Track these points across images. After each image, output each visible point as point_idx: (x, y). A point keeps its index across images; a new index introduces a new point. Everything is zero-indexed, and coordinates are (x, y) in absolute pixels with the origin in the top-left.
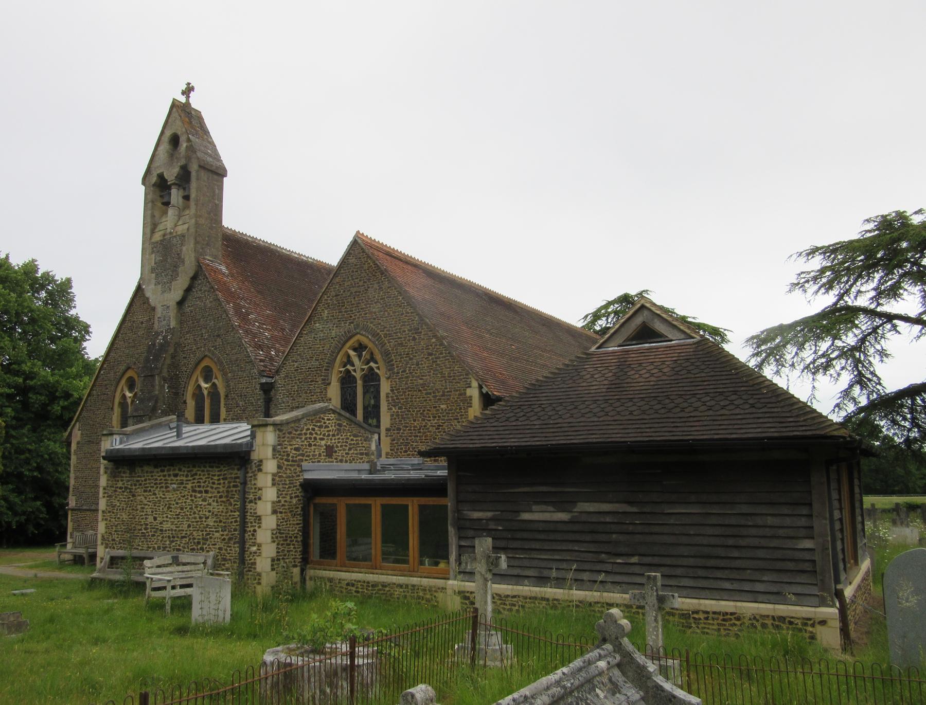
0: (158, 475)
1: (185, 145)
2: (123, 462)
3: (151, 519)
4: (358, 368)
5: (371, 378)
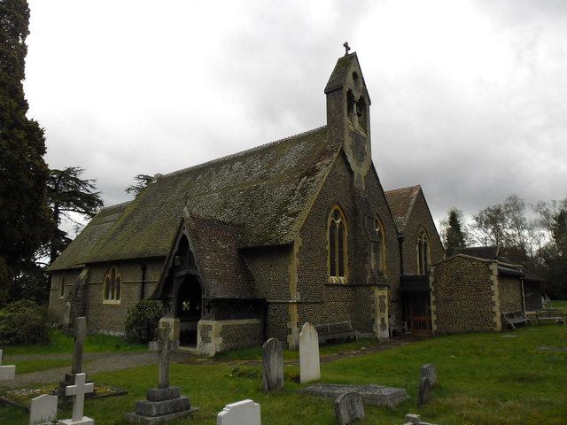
5: (425, 245)
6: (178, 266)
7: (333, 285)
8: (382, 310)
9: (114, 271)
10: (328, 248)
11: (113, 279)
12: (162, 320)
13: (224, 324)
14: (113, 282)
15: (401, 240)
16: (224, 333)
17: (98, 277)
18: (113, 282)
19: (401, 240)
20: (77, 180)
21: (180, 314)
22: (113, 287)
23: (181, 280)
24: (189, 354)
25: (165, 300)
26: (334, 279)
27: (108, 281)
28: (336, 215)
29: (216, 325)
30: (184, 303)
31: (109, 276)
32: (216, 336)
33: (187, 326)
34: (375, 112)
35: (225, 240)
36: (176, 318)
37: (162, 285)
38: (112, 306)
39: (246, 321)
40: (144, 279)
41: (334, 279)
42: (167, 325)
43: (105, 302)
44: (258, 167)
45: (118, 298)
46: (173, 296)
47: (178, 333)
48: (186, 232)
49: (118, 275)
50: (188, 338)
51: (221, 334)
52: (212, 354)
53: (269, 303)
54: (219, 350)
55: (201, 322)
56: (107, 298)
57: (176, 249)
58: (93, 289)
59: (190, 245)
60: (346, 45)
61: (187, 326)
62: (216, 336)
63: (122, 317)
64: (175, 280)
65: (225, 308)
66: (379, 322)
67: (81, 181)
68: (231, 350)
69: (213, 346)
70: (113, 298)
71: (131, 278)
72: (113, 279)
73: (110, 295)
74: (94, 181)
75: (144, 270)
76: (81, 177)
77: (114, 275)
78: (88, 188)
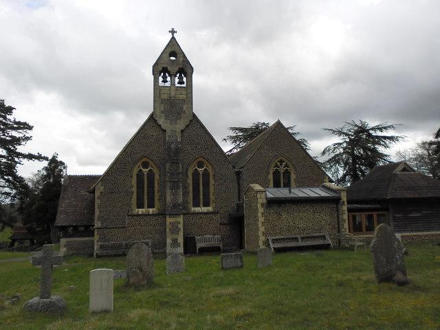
0: (294, 207)
1: (182, 59)
2: (271, 203)
3: (291, 224)
4: (282, 169)
7: (138, 215)
10: (134, 189)
15: (238, 174)
19: (238, 174)
26: (141, 211)
28: (200, 165)
34: (196, 78)
39: (87, 238)
41: (141, 211)
60: (173, 32)
66: (169, 241)
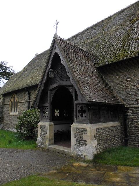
6: (52, 78)
8: (134, 117)
9: (14, 97)
11: (14, 101)
12: (40, 123)
13: (97, 127)
14: (14, 103)
16: (98, 136)
17: (8, 100)
18: (14, 103)
20: (5, 67)
21: (53, 119)
22: (14, 105)
23: (55, 91)
24: (63, 153)
25: (42, 108)
27: (12, 103)
29: (91, 128)
30: (55, 111)
31: (12, 100)
32: (92, 139)
33: (60, 128)
35: (88, 61)
36: (50, 122)
37: (39, 96)
38: (13, 115)
39: (111, 124)
40: (29, 100)
42: (43, 127)
43: (11, 114)
44: (94, 33)
45: (17, 111)
46: (47, 104)
47: (53, 134)
48: (57, 51)
49: (16, 99)
50: (62, 137)
51: (96, 137)
52: (90, 157)
53: (128, 108)
54: (95, 153)
55: (74, 126)
56: (12, 112)
57: (50, 66)
58: (6, 107)
59: (62, 59)
61: (60, 128)
62: (92, 139)
63: (17, 122)
64: (49, 92)
65: (97, 111)
67: (7, 67)
68: (105, 151)
69: (89, 149)
70: (14, 112)
71: (23, 98)
72: (14, 101)
73: (13, 110)
74: (12, 67)
75: (29, 94)
76: (7, 66)
77: (14, 99)
78: (10, 70)
